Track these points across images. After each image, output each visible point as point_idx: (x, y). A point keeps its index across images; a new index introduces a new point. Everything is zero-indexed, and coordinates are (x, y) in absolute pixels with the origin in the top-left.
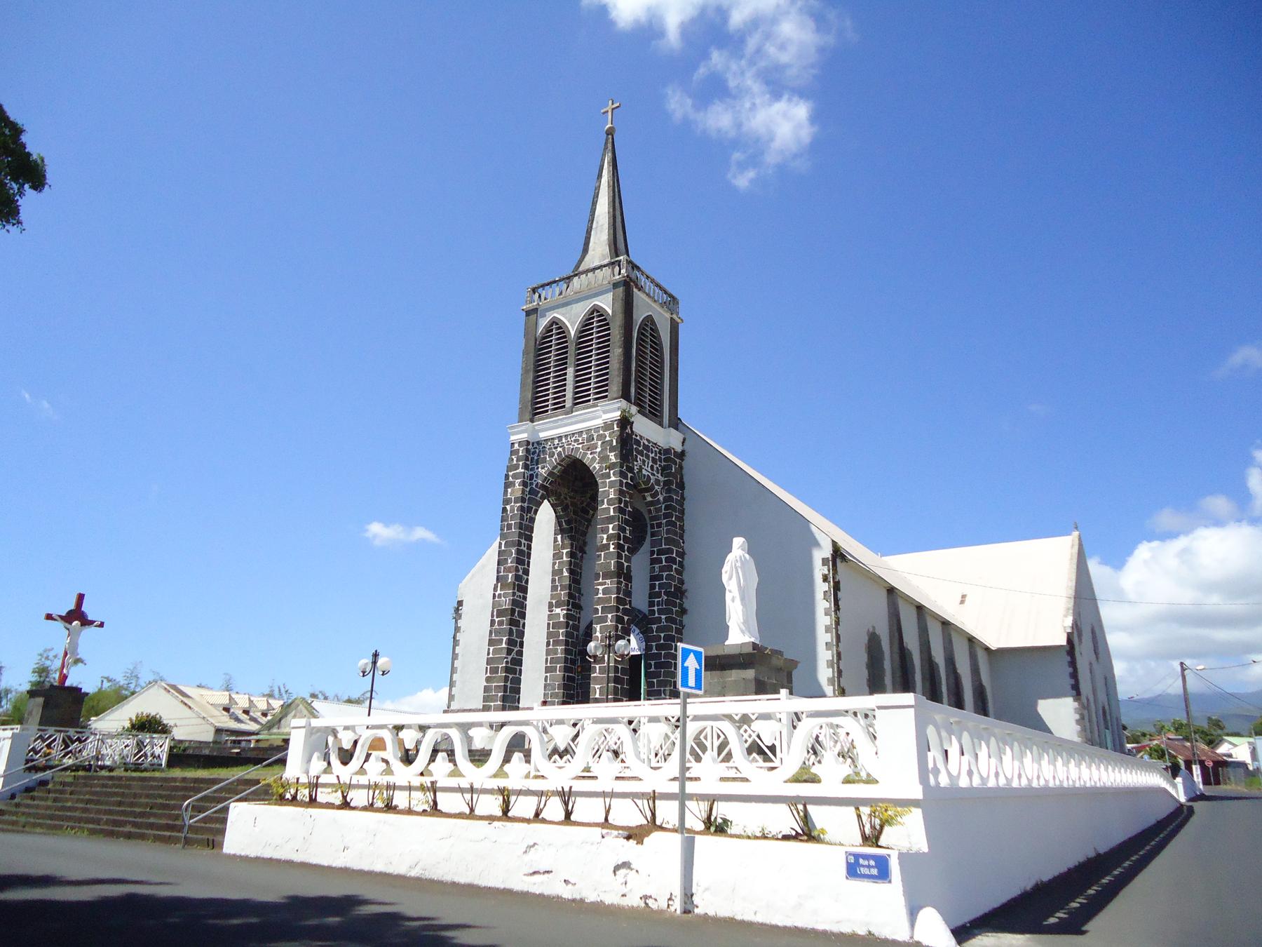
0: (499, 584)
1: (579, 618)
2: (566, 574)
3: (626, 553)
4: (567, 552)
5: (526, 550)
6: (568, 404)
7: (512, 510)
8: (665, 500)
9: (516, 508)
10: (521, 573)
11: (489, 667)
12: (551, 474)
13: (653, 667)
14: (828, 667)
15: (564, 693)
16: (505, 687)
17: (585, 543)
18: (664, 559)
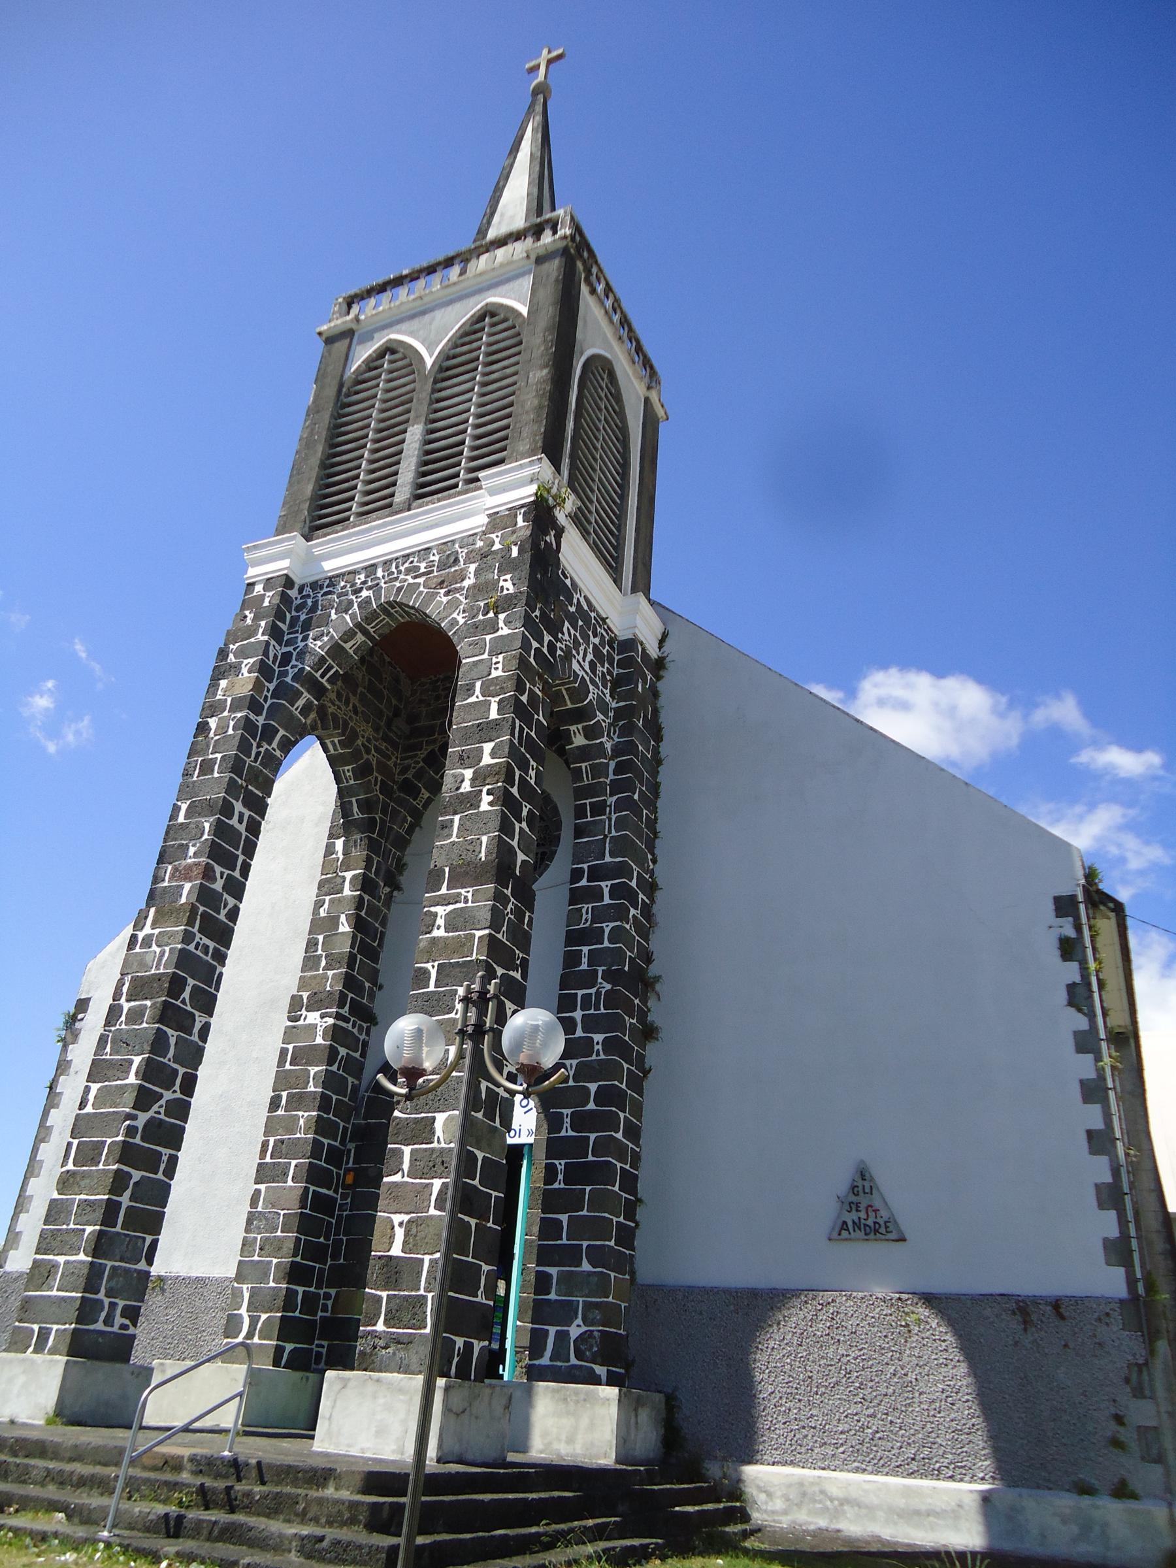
0: (153, 910)
1: (365, 1044)
2: (345, 927)
3: (524, 825)
4: (354, 877)
5: (244, 834)
6: (402, 492)
7: (222, 728)
8: (617, 751)
9: (232, 723)
10: (218, 886)
11: (76, 1142)
12: (336, 650)
13: (560, 1177)
14: (1101, 1206)
15: (298, 1240)
16: (111, 1208)
17: (401, 866)
18: (606, 892)
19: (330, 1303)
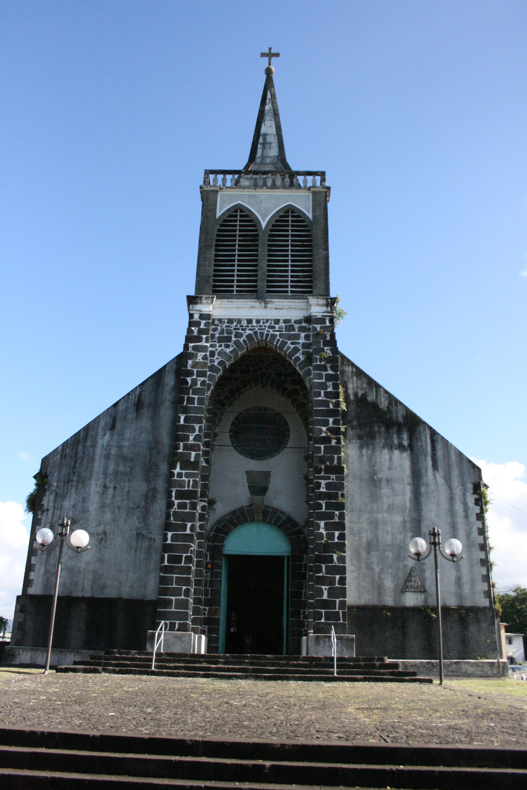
19: (206, 612)
